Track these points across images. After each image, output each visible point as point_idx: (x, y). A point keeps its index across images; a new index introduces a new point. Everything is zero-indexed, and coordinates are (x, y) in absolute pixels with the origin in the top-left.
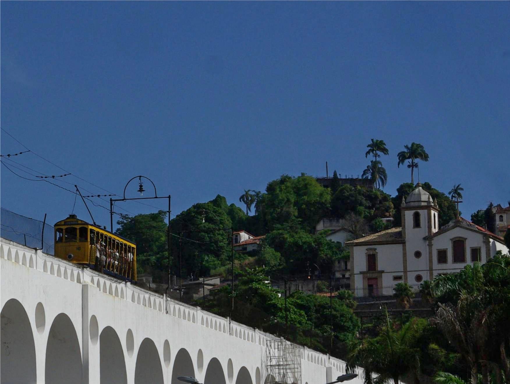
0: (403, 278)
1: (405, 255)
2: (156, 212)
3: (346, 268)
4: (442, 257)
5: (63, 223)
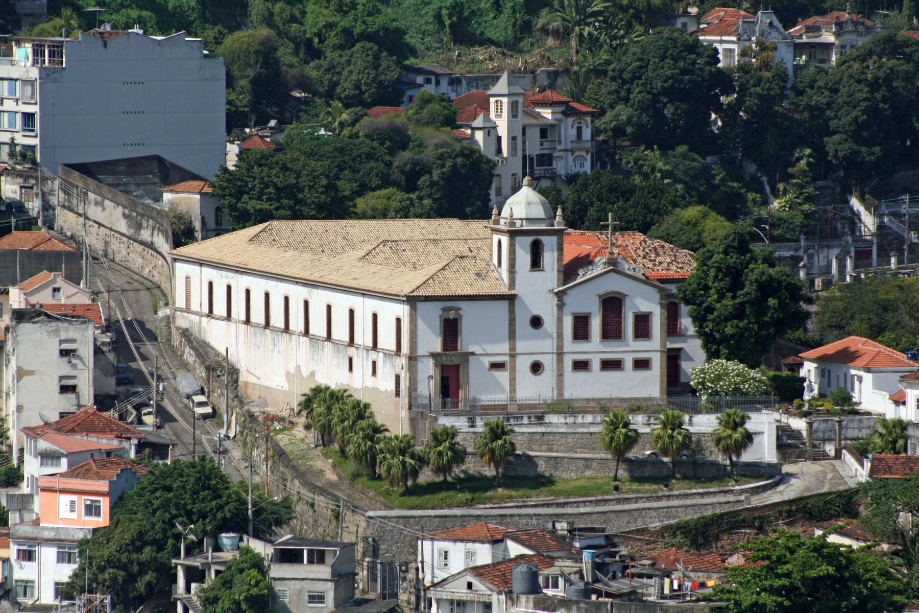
0: (508, 366)
3: (451, 330)
4: (581, 329)
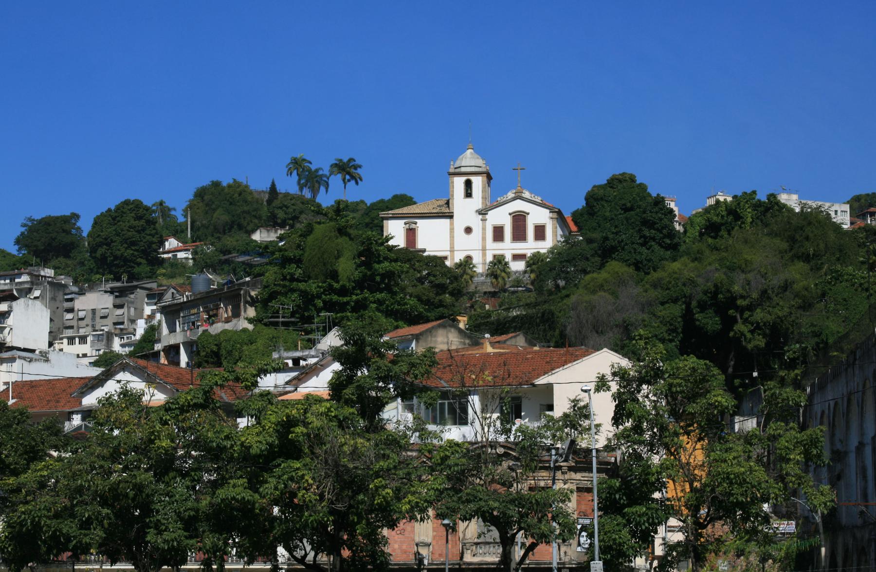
1: (452, 230)
2: (68, 213)
5: (838, 446)
